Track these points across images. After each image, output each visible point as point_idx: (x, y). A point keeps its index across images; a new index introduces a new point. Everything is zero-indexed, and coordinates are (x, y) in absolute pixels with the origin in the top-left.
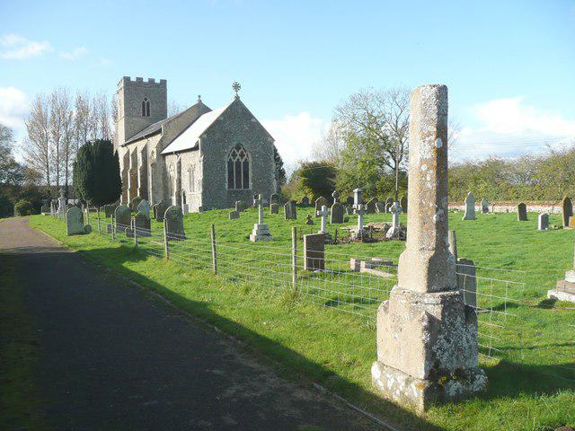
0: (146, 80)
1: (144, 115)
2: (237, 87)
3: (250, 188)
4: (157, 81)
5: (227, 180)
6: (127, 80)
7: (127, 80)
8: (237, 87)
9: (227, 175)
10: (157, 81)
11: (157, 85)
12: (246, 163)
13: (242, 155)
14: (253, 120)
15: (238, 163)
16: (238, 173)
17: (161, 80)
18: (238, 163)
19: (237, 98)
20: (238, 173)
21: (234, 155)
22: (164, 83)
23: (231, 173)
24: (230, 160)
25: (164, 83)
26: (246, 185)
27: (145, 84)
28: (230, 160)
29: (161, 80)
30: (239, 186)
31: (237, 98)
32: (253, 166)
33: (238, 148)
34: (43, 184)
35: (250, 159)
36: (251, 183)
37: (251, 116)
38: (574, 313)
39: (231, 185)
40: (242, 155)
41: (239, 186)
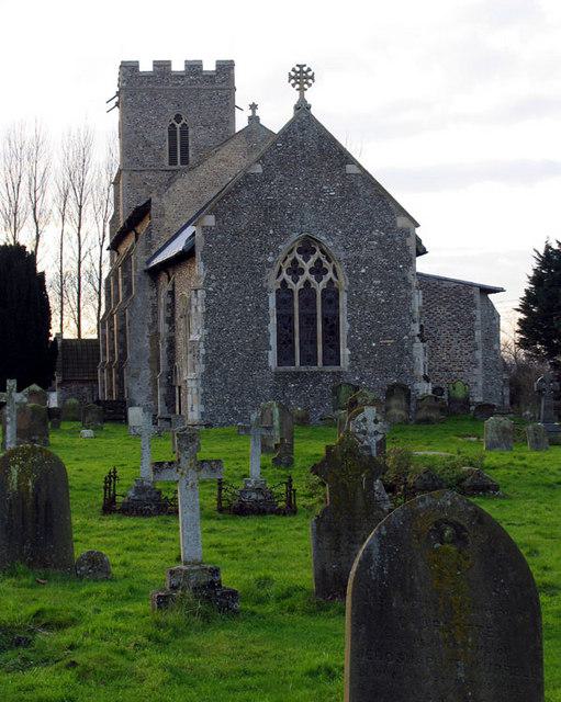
0: (178, 66)
1: (173, 161)
2: (301, 77)
3: (345, 362)
4: (209, 66)
5: (273, 341)
6: (129, 70)
7: (129, 70)
8: (301, 77)
9: (272, 327)
10: (209, 66)
11: (210, 77)
12: (331, 296)
13: (318, 270)
14: (350, 169)
15: (308, 292)
16: (309, 320)
17: (157, 64)
18: (308, 292)
19: (302, 108)
20: (309, 320)
21: (296, 271)
22: (226, 69)
23: (285, 322)
24: (284, 283)
25: (226, 69)
26: (333, 357)
27: (179, 76)
28: (307, 283)
29: (157, 64)
30: (309, 359)
31: (302, 108)
32: (351, 302)
33: (307, 248)
34: (73, 518)
35: (343, 282)
36: (345, 352)
37: (344, 158)
38: (559, 479)
39: (285, 355)
40: (318, 270)
41: (309, 359)
